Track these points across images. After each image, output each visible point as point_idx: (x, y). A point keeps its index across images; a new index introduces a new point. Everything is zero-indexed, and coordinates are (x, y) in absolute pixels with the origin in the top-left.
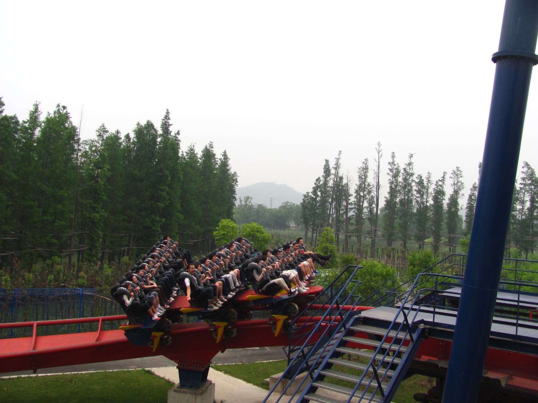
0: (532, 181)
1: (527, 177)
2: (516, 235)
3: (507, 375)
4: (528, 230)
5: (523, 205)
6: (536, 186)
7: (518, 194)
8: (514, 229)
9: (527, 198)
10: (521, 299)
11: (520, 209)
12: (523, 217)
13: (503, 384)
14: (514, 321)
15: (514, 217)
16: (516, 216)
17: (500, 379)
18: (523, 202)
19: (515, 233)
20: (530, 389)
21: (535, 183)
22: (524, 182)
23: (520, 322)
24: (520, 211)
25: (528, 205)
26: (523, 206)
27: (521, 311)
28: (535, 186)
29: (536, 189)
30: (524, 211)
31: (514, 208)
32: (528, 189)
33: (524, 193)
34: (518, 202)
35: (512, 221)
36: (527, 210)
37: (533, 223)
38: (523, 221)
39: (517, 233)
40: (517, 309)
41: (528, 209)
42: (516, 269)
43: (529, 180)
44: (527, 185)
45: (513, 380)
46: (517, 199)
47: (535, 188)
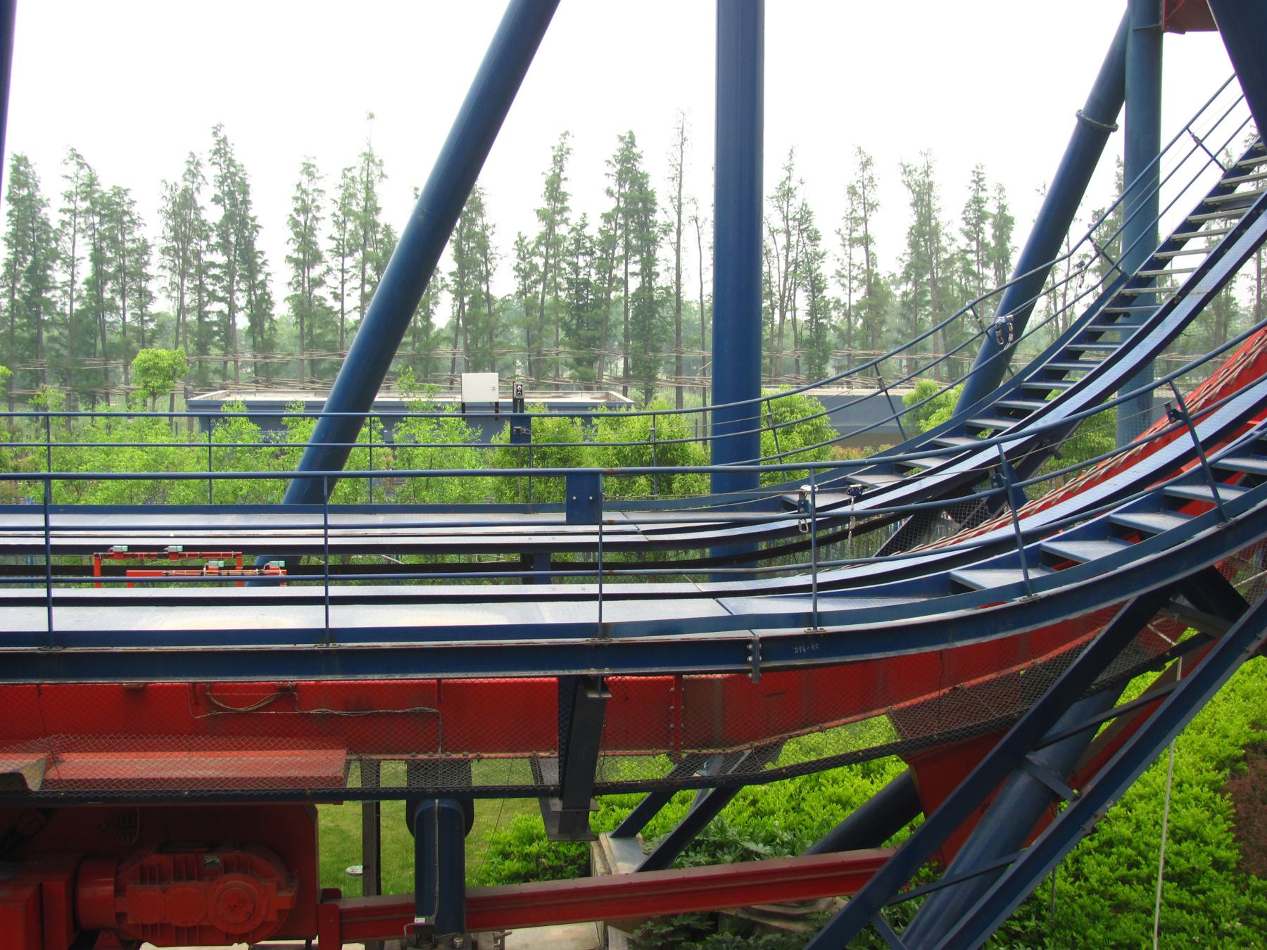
0: (92, 203)
1: (79, 190)
2: (59, 356)
3: (42, 756)
4: (93, 341)
5: (72, 272)
6: (105, 216)
7: (57, 240)
8: (53, 339)
9: (83, 249)
10: (53, 523)
11: (65, 284)
12: (77, 306)
13: (34, 784)
14: (40, 592)
15: (50, 305)
16: (56, 302)
17: (23, 772)
18: (71, 263)
19: (57, 351)
20: (127, 781)
21: (103, 209)
22: (72, 206)
23: (57, 592)
24: (66, 288)
25: (85, 270)
26: (72, 275)
27: (56, 560)
28: (102, 216)
29: (106, 226)
30: (77, 287)
31: (49, 282)
32: (84, 226)
33: (74, 235)
34: (59, 262)
35: (46, 318)
36: (85, 286)
37: (105, 322)
38: (79, 317)
39: (65, 352)
40: (44, 558)
41: (87, 282)
42: (48, 439)
43: (83, 199)
44: (80, 212)
45: (61, 767)
46: (55, 255)
47: (101, 223)
